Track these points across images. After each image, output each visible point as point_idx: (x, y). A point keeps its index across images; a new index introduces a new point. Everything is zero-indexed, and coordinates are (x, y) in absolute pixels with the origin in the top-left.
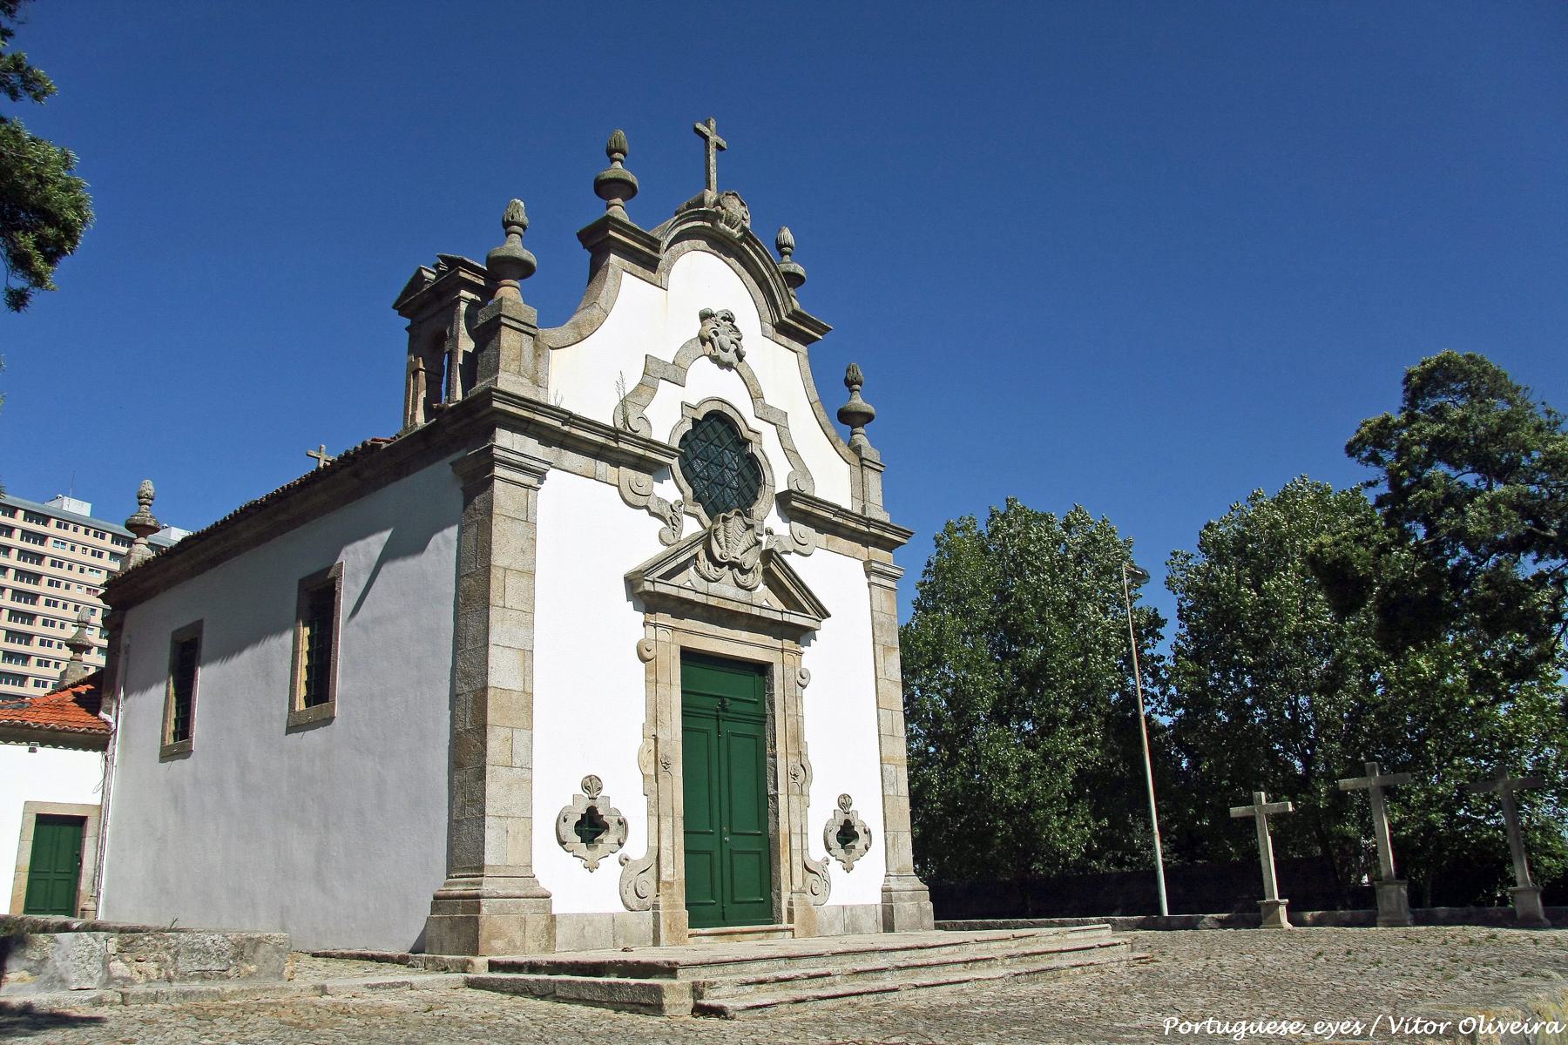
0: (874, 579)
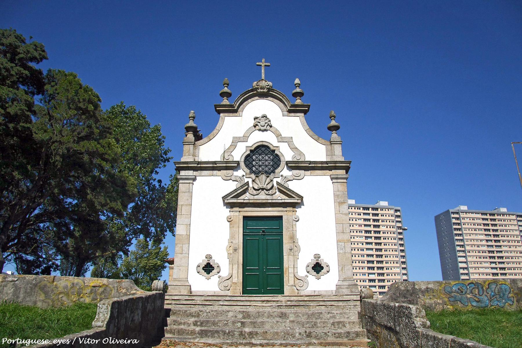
0: (334, 181)
